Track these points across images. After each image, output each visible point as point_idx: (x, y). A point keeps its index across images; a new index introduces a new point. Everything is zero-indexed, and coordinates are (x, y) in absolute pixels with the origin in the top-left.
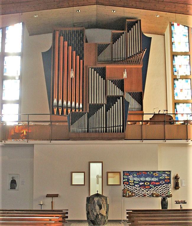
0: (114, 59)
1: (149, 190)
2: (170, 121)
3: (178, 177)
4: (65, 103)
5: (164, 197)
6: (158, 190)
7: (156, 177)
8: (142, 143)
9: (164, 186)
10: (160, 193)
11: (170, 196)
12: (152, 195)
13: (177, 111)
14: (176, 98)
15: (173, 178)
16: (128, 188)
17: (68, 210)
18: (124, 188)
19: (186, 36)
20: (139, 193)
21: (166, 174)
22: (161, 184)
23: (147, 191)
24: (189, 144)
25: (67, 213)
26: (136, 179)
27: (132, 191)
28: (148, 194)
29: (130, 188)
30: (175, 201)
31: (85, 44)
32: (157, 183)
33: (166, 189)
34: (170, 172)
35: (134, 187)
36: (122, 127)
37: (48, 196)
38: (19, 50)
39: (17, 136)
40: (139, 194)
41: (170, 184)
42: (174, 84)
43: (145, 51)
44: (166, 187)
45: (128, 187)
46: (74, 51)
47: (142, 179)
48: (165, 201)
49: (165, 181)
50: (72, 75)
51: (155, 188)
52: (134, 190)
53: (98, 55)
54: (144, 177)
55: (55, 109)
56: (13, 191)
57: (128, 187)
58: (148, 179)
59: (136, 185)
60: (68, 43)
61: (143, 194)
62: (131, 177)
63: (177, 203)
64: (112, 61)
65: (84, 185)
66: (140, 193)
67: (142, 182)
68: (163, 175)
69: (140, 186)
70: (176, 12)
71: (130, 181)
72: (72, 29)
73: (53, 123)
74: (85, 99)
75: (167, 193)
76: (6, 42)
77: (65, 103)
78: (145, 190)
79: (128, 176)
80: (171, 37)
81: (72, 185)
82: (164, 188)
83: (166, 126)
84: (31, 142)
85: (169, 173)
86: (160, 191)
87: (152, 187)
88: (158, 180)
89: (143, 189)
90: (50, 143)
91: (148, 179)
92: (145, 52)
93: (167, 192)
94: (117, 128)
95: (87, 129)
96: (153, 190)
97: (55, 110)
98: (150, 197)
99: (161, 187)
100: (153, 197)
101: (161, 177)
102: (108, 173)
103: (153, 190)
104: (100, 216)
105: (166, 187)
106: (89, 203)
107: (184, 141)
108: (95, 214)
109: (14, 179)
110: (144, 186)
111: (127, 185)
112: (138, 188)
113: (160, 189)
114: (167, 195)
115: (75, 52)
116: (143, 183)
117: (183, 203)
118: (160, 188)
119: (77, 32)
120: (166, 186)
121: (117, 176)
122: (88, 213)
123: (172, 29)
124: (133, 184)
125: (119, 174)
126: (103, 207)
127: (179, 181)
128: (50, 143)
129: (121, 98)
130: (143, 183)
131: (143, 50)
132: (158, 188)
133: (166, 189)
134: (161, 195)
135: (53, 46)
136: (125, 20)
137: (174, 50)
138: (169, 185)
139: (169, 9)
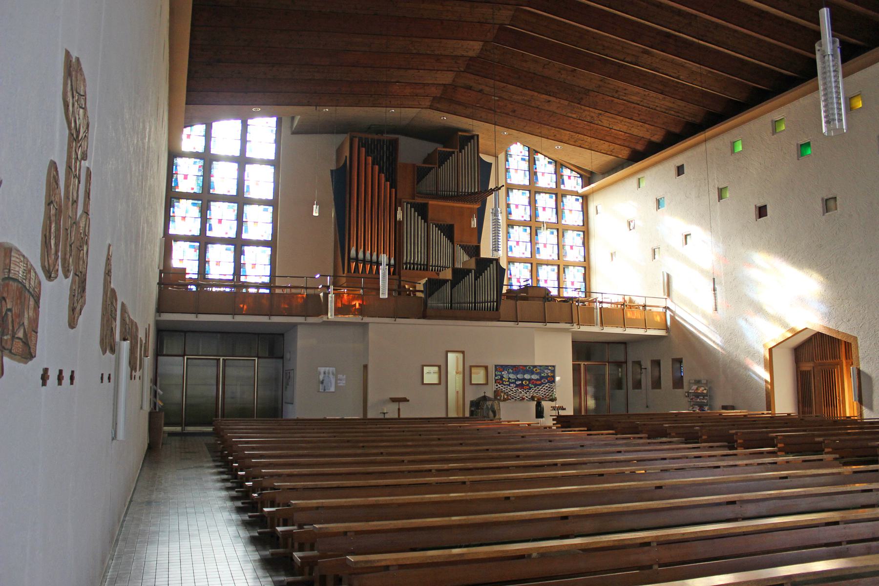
1: (527, 391)
6: (539, 392)
7: (537, 374)
10: (543, 396)
13: (511, 275)
16: (502, 389)
18: (497, 389)
21: (549, 370)
22: (543, 383)
23: (526, 393)
26: (512, 376)
33: (549, 390)
34: (554, 366)
40: (515, 397)
44: (549, 388)
45: (501, 388)
47: (520, 376)
57: (501, 388)
58: (527, 376)
59: (511, 385)
62: (505, 374)
68: (546, 371)
71: (504, 379)
75: (551, 396)
78: (523, 391)
79: (501, 372)
81: (423, 383)
82: (546, 388)
84: (366, 320)
86: (541, 392)
88: (539, 378)
89: (520, 391)
91: (527, 376)
93: (550, 394)
99: (544, 388)
102: (471, 367)
105: (549, 388)
110: (521, 386)
111: (500, 385)
112: (514, 389)
113: (542, 390)
116: (520, 382)
120: (549, 386)
124: (507, 383)
130: (520, 382)
133: (549, 390)
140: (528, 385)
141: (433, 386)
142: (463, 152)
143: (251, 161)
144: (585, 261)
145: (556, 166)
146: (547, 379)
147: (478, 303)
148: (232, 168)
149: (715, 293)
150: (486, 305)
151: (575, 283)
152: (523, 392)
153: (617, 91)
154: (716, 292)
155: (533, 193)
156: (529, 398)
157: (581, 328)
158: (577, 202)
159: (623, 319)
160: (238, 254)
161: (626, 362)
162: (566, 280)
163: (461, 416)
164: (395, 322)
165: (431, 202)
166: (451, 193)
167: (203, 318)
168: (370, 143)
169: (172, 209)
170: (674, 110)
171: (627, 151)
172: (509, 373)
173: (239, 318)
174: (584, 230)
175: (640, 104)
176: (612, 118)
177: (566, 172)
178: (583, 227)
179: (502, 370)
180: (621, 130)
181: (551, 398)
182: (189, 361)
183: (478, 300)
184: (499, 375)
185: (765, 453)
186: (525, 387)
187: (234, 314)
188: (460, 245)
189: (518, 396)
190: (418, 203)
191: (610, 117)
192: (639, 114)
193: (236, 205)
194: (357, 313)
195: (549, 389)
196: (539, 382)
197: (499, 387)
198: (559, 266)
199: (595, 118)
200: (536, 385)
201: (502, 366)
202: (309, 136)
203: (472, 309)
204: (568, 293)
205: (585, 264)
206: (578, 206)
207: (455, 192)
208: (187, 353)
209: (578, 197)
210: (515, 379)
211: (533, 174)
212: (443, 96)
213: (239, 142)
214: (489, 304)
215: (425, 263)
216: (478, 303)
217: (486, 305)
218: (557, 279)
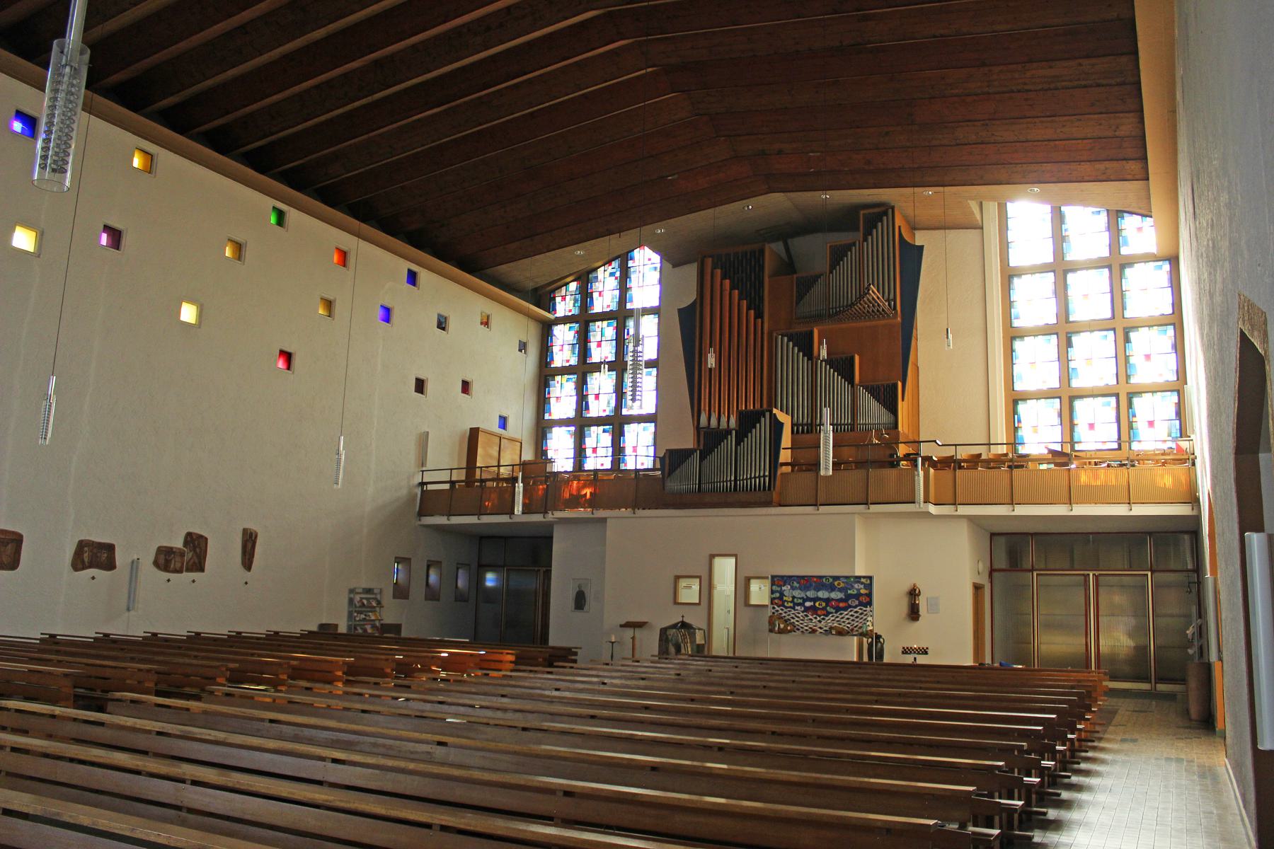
1: (823, 619)
7: (840, 590)
9: (855, 610)
16: (781, 614)
18: (773, 613)
20: (801, 626)
21: (862, 583)
22: (850, 606)
26: (797, 593)
28: (821, 628)
29: (785, 612)
33: (862, 618)
34: (870, 578)
35: (793, 612)
36: (767, 479)
40: (802, 628)
44: (861, 614)
45: (781, 612)
47: (810, 594)
50: (711, 361)
51: (838, 615)
54: (815, 590)
56: (579, 614)
59: (796, 608)
61: (810, 628)
65: (699, 604)
68: (856, 586)
69: (807, 609)
71: (785, 598)
75: (861, 627)
78: (816, 618)
79: (781, 586)
81: (676, 603)
82: (856, 615)
84: (601, 513)
86: (847, 621)
87: (832, 613)
88: (844, 597)
89: (811, 617)
93: (860, 625)
96: (833, 620)
99: (850, 613)
101: (850, 590)
103: (833, 618)
105: (861, 614)
110: (814, 610)
111: (779, 607)
112: (802, 614)
116: (812, 603)
118: (847, 614)
120: (860, 611)
124: (791, 605)
128: (634, 516)
130: (812, 603)
138: (868, 609)
140: (824, 609)
142: (870, 240)
144: (1178, 379)
146: (858, 599)
148: (1101, 278)
150: (729, 485)
155: (1116, 269)
156: (826, 631)
157: (820, 509)
158: (1159, 272)
159: (1068, 488)
163: (731, 655)
164: (818, 512)
166: (834, 311)
172: (793, 588)
173: (486, 519)
174: (1172, 322)
178: (1173, 316)
179: (782, 583)
181: (860, 631)
187: (480, 514)
189: (806, 626)
192: (1031, 105)
193: (614, 373)
194: (586, 505)
195: (857, 620)
197: (777, 611)
198: (1117, 395)
200: (838, 609)
201: (782, 577)
202: (685, 267)
203: (730, 490)
209: (1161, 263)
210: (803, 598)
215: (809, 421)
217: (729, 485)
218: (1117, 420)
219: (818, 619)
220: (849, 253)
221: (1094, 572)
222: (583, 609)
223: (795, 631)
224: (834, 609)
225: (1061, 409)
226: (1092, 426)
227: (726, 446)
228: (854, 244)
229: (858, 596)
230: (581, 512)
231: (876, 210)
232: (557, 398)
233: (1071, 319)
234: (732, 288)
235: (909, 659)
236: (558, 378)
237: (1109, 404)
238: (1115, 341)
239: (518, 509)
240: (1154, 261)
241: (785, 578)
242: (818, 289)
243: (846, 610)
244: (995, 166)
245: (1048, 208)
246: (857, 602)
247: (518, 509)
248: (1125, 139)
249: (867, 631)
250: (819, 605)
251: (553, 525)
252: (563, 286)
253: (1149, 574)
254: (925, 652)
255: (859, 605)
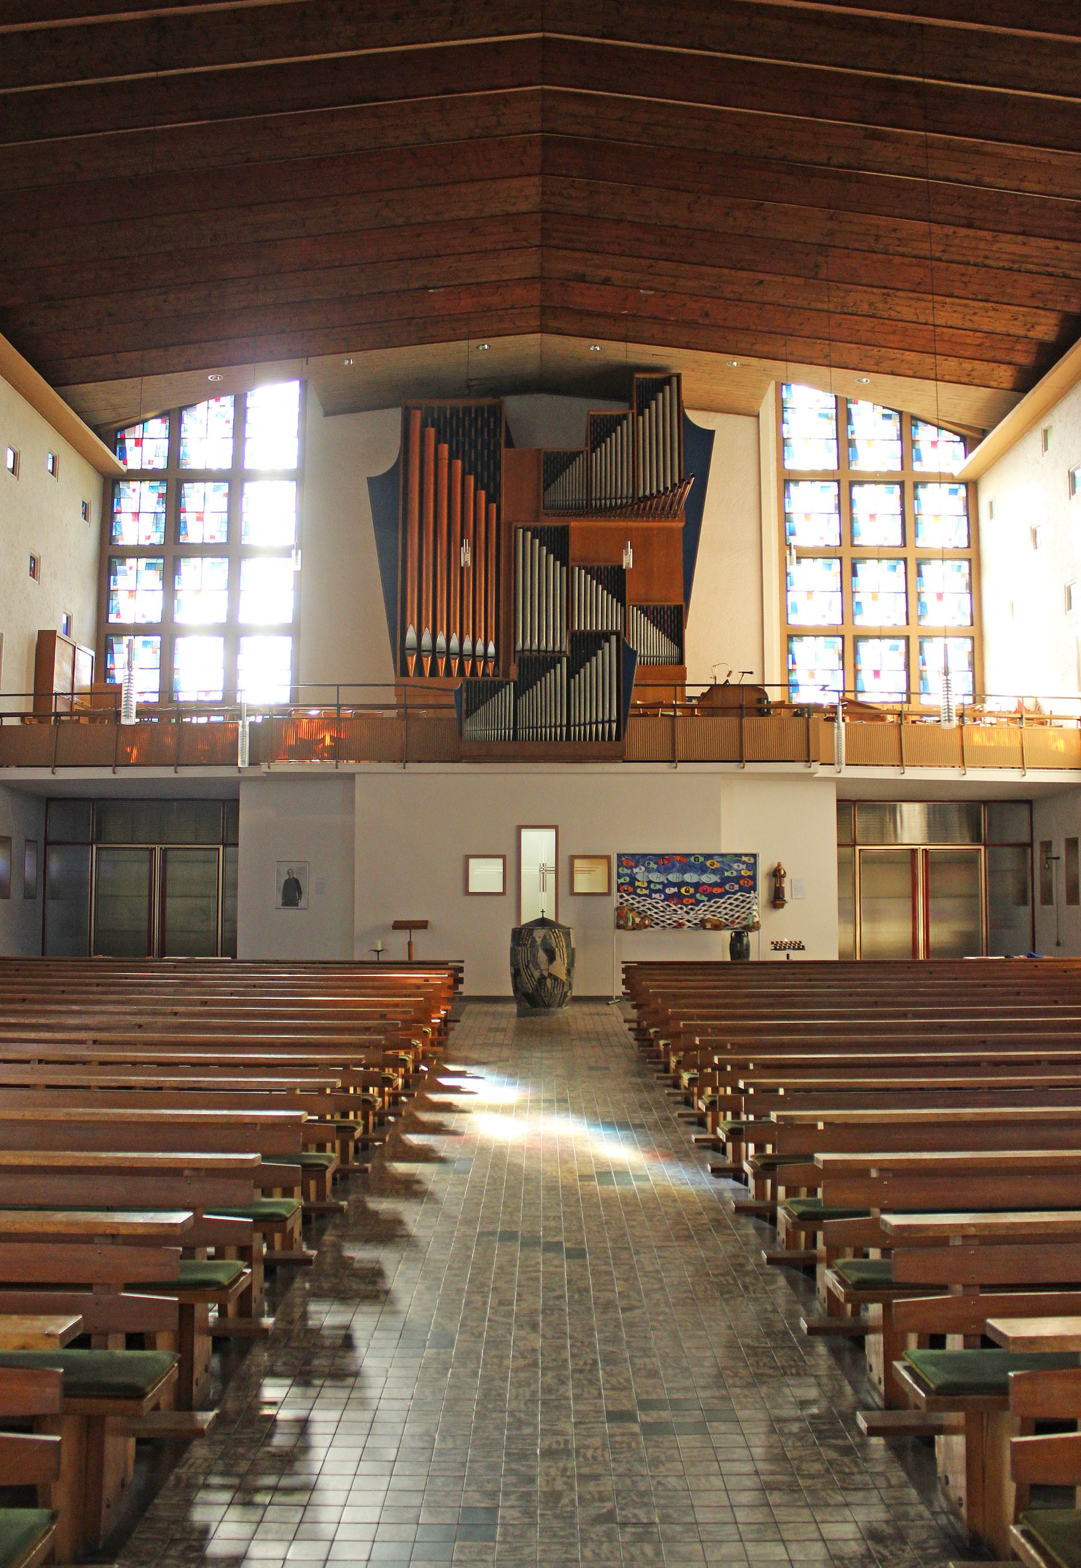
0: (594, 502)
1: (692, 909)
2: (759, 706)
3: (782, 872)
4: (441, 640)
5: (736, 928)
6: (719, 910)
7: (714, 872)
8: (674, 771)
9: (735, 897)
10: (726, 919)
11: (755, 927)
12: (702, 924)
13: (794, 663)
14: (793, 620)
15: (768, 874)
16: (632, 904)
17: (462, 962)
18: (621, 903)
19: (828, 418)
20: (662, 919)
21: (744, 863)
22: (728, 893)
23: (687, 913)
24: (815, 773)
25: (461, 970)
26: (655, 877)
27: (643, 911)
28: (689, 921)
29: (639, 902)
30: (772, 943)
31: (504, 450)
32: (716, 890)
33: (743, 907)
34: (754, 856)
35: (649, 901)
36: (614, 725)
37: (398, 926)
38: (290, 460)
39: (306, 749)
40: (663, 921)
41: (755, 890)
42: (787, 574)
43: (689, 483)
44: (743, 901)
45: (632, 901)
46: (470, 474)
47: (673, 877)
48: (741, 942)
49: (741, 882)
50: (466, 557)
51: (711, 903)
52: (649, 909)
53: (545, 489)
54: (679, 871)
55: (409, 659)
56: (290, 913)
57: (632, 901)
58: (690, 877)
59: (654, 896)
60: (450, 449)
61: (674, 922)
62: (639, 872)
63: (775, 949)
64: (587, 509)
65: (503, 894)
66: (668, 917)
67: (674, 885)
68: (735, 866)
69: (668, 898)
70: (790, 357)
71: (637, 884)
72: (460, 403)
73: (409, 711)
74: (505, 633)
75: (745, 919)
76: (247, 435)
77: (441, 640)
78: (681, 908)
79: (631, 868)
80: (781, 421)
81: (467, 893)
82: (736, 903)
83: (745, 720)
84: (349, 766)
85: (752, 861)
86: (724, 912)
87: (703, 901)
88: (719, 881)
89: (674, 907)
90: (404, 771)
91: (690, 877)
92: (689, 487)
93: (744, 916)
94: (600, 726)
95: (512, 731)
96: (705, 911)
97: (412, 661)
98: (696, 930)
99: (729, 901)
100: (705, 928)
101: (727, 871)
102: (573, 858)
103: (704, 908)
104: (549, 982)
105: (743, 901)
106: (518, 945)
107: (799, 767)
108: (537, 974)
109: (295, 876)
110: (678, 898)
111: (628, 895)
112: (661, 904)
113: (724, 906)
114: (745, 923)
115: (472, 477)
116: (676, 890)
117: (794, 949)
118: (724, 903)
119: (479, 410)
120: (742, 898)
121: (601, 869)
122: (516, 974)
123: (785, 395)
124: (647, 892)
125: (605, 862)
126: (558, 958)
127: (786, 884)
128: (404, 771)
129: (614, 638)
130: (676, 890)
131: (684, 480)
132: (718, 904)
133: (743, 907)
134: (727, 925)
135: (402, 457)
136: (632, 378)
137: (789, 465)
138: (752, 895)
139: (766, 348)
140: (693, 896)
141: (595, 898)
143: (860, 480)
144: (972, 625)
145: (901, 422)
147: (575, 726)
149: (947, 680)
151: (817, 673)
152: (680, 912)
153: (877, 238)
154: (949, 678)
155: (845, 485)
158: (954, 497)
160: (233, 648)
161: (1031, 845)
162: (795, 667)
165: (573, 524)
166: (608, 502)
167: (65, 774)
168: (448, 416)
169: (112, 577)
170: (1035, 260)
171: (1006, 371)
173: (124, 773)
175: (944, 258)
176: (918, 299)
177: (925, 434)
179: (633, 864)
180: (949, 323)
182: (104, 853)
183: (575, 718)
184: (627, 875)
185: (985, 1064)
186: (685, 901)
188: (640, 608)
190: (550, 528)
191: (911, 299)
192: (964, 283)
195: (742, 905)
196: (719, 890)
198: (907, 638)
199: (880, 306)
201: (634, 855)
204: (803, 697)
205: (972, 632)
206: (956, 502)
207: (627, 497)
208: (859, 840)
209: (956, 486)
210: (662, 883)
211: (845, 444)
212: (547, 304)
213: (230, 443)
214: (600, 726)
216: (575, 726)
219: (685, 909)
220: (619, 428)
221: (161, 846)
222: (297, 905)
223: (652, 927)
224: (706, 896)
225: (843, 651)
226: (877, 673)
227: (553, 678)
228: (625, 417)
229: (738, 879)
230: (315, 765)
231: (655, 376)
232: (131, 591)
233: (856, 542)
234: (452, 456)
235: (781, 956)
236: (131, 562)
237: (896, 648)
238: (841, 572)
239: (243, 761)
240: (949, 483)
241: (637, 857)
242: (576, 471)
243: (721, 898)
244: (819, 341)
245: (829, 400)
246: (737, 887)
247: (243, 761)
248: (1021, 340)
249: (753, 923)
250: (686, 891)
251: (239, 783)
252: (138, 423)
253: (221, 847)
254: (800, 947)
255: (740, 890)
